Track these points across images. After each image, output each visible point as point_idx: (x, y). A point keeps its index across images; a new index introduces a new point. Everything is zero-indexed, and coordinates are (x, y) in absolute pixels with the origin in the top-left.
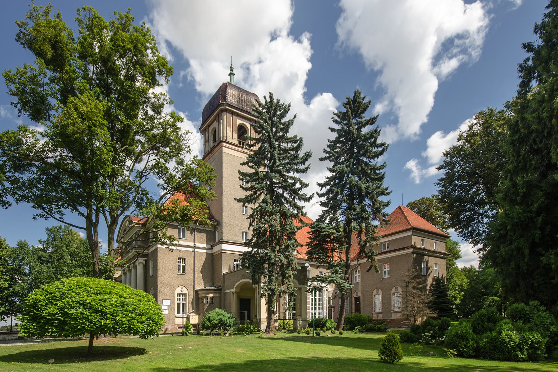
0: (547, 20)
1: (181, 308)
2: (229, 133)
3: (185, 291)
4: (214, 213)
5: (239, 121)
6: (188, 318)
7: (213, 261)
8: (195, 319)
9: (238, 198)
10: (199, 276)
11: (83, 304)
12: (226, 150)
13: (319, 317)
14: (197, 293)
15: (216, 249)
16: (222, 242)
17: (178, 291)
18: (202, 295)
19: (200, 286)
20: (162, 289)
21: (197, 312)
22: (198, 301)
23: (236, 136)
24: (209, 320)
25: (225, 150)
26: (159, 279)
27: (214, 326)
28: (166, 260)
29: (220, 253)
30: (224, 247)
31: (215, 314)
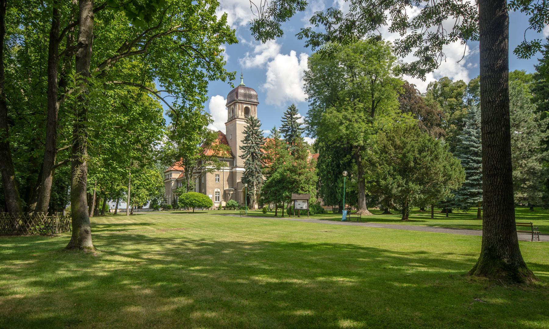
0: (500, 13)
1: (217, 199)
2: (240, 113)
3: (219, 190)
4: (233, 151)
5: (245, 106)
6: (221, 203)
7: (232, 176)
8: (224, 204)
9: (297, 59)
10: (226, 183)
11: (195, 200)
12: (238, 122)
13: (478, 217)
14: (225, 191)
15: (234, 170)
16: (236, 167)
17: (216, 190)
18: (227, 192)
19: (227, 188)
20: (209, 190)
21: (225, 201)
22: (225, 195)
23: (243, 114)
24: (228, 204)
25: (237, 122)
26: (207, 185)
27: (230, 206)
28: (210, 178)
29: (236, 172)
30: (238, 169)
31: (232, 202)
